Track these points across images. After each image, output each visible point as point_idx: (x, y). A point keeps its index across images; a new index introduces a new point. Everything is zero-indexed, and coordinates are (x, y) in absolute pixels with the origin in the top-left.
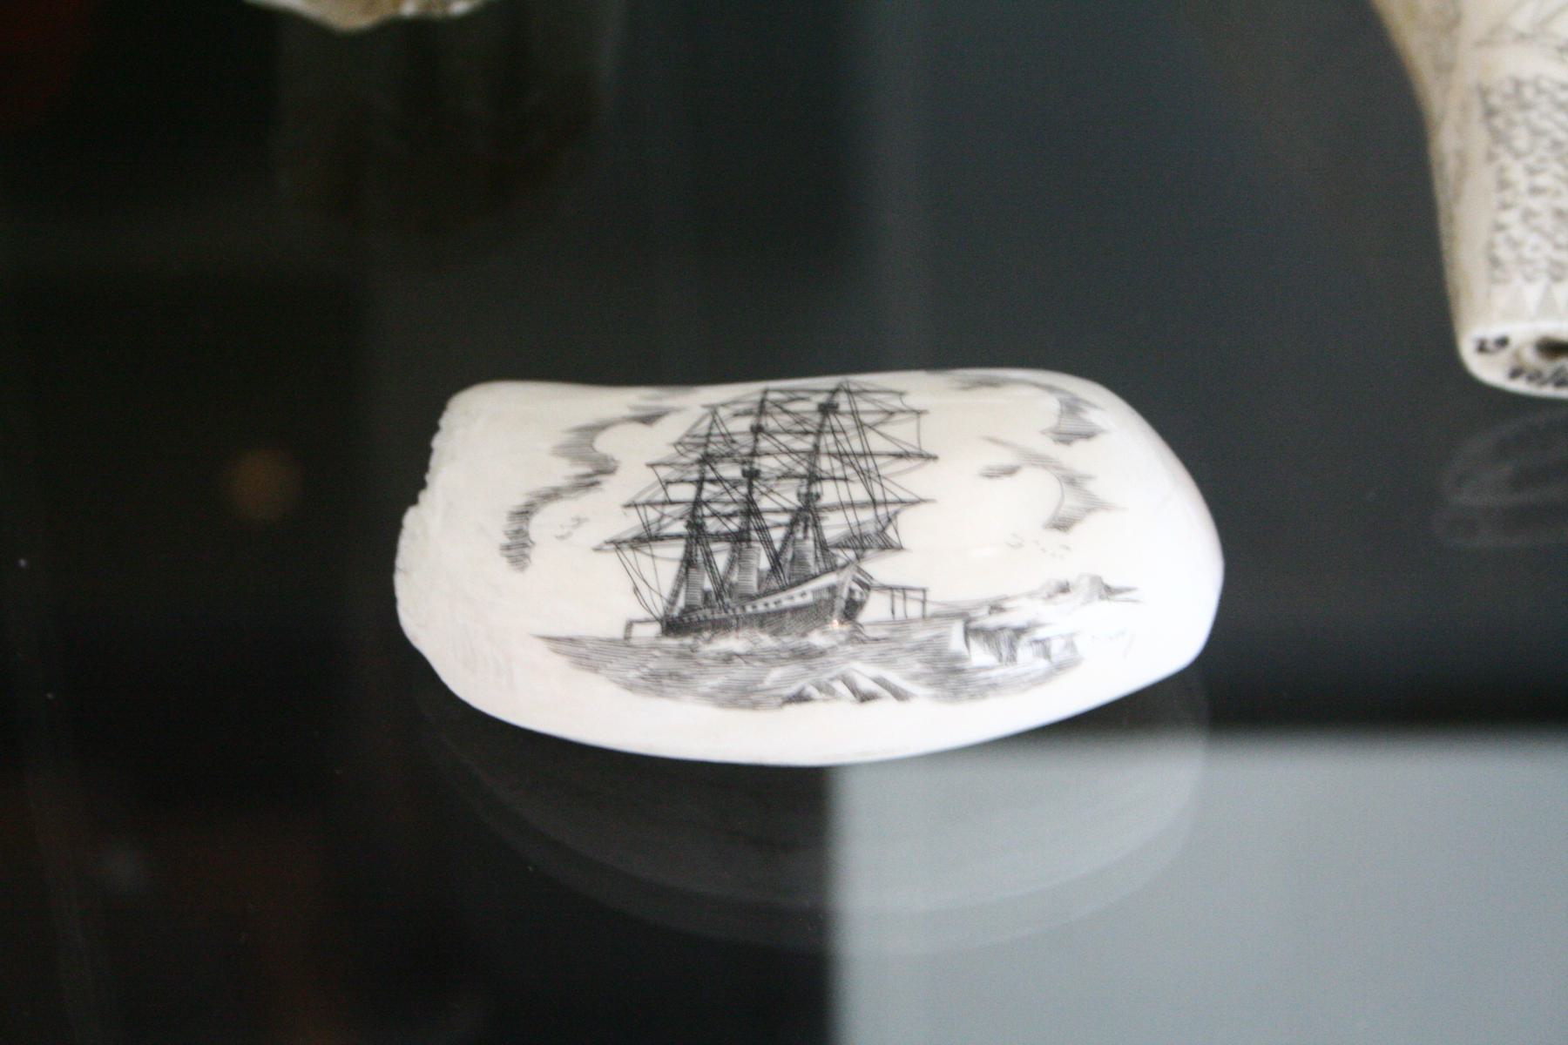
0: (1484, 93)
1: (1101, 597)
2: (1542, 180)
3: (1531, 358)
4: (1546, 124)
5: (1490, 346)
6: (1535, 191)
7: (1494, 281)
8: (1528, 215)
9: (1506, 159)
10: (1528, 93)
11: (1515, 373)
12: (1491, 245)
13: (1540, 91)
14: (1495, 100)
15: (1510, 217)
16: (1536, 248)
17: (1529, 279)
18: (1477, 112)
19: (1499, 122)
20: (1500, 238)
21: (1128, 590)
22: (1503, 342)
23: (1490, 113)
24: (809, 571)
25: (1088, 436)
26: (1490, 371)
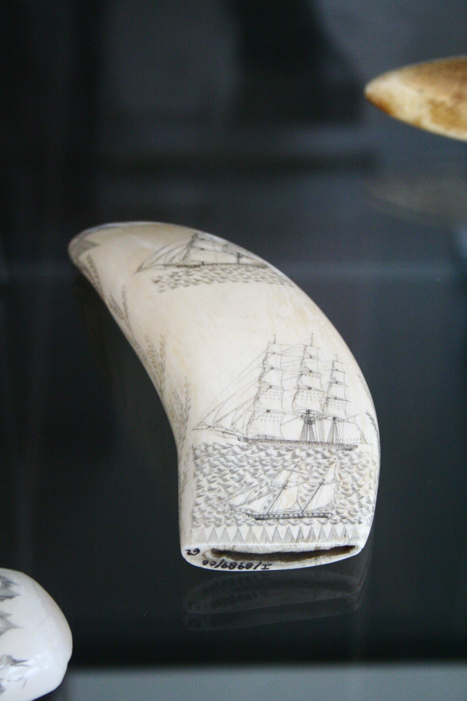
0: (194, 449)
1: (12, 665)
2: (214, 485)
3: (210, 556)
4: (217, 463)
5: (192, 552)
6: (211, 490)
7: (194, 526)
8: (208, 499)
9: (201, 477)
10: (210, 449)
11: (205, 563)
12: (193, 512)
13: (215, 449)
14: (198, 452)
15: (201, 500)
16: (210, 513)
17: (207, 526)
18: (191, 457)
19: (198, 461)
20: (196, 509)
21: (23, 661)
22: (198, 551)
23: (196, 458)
24: (79, 254)
25: (11, 597)
26: (195, 561)
